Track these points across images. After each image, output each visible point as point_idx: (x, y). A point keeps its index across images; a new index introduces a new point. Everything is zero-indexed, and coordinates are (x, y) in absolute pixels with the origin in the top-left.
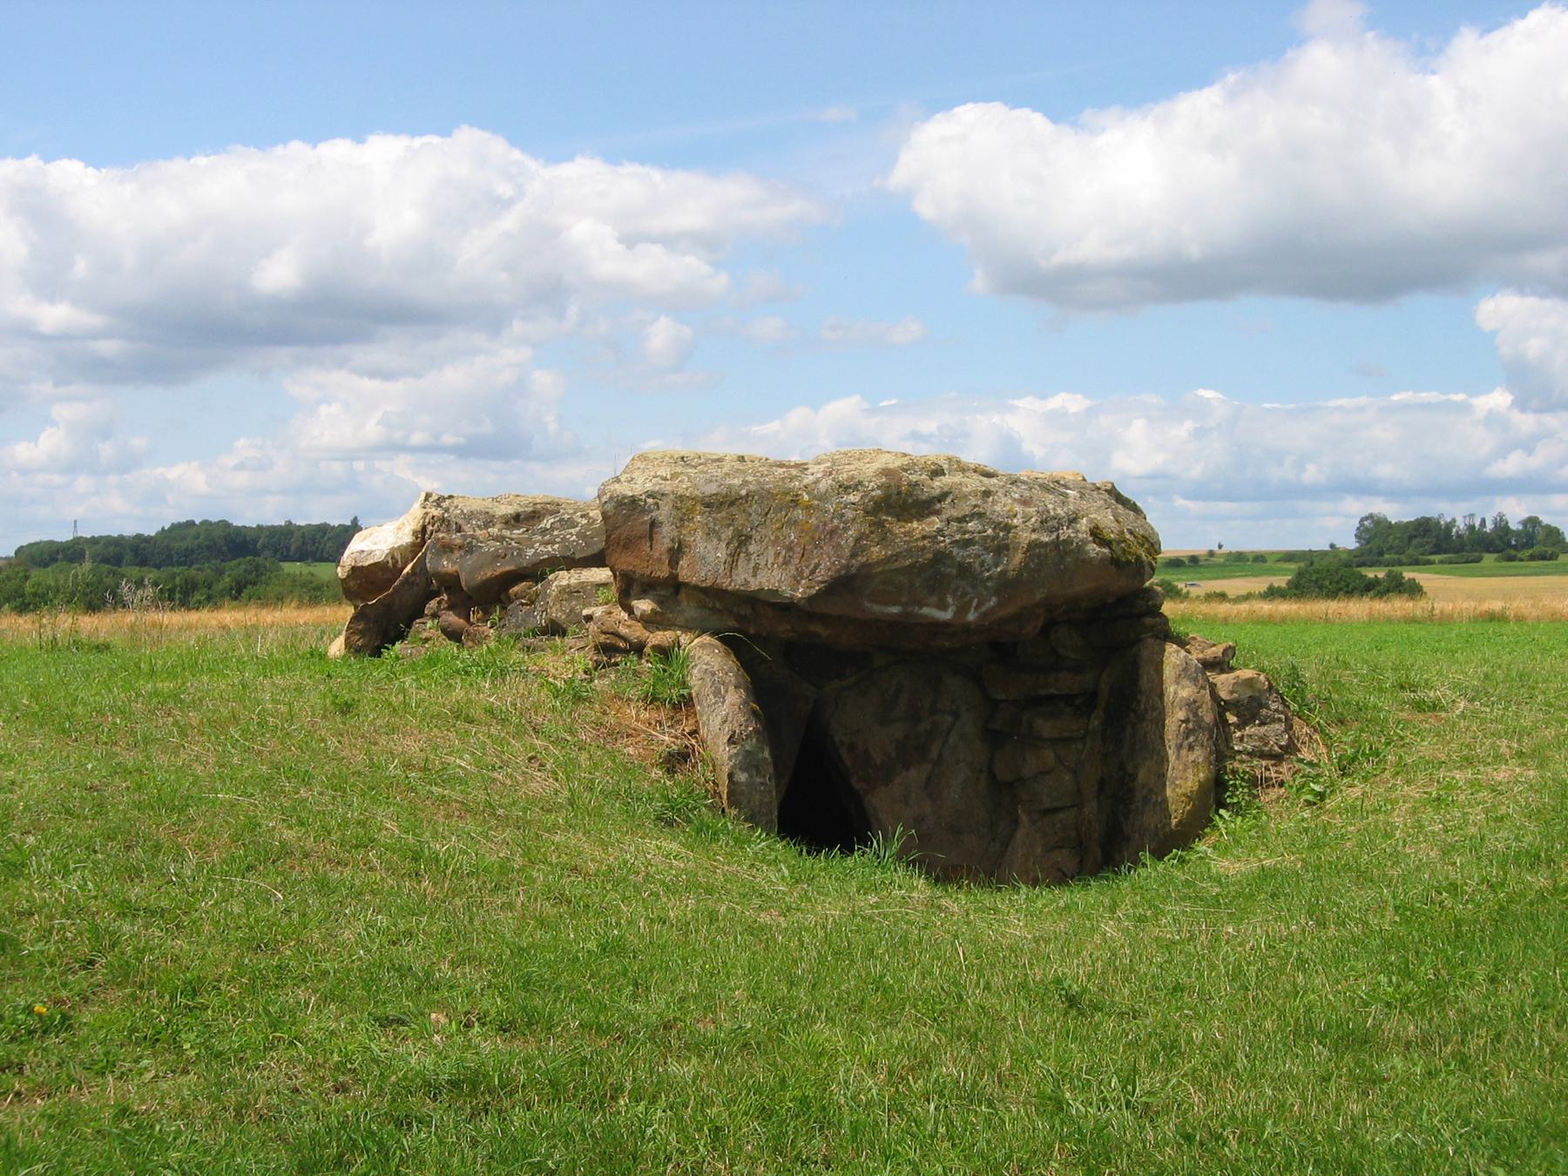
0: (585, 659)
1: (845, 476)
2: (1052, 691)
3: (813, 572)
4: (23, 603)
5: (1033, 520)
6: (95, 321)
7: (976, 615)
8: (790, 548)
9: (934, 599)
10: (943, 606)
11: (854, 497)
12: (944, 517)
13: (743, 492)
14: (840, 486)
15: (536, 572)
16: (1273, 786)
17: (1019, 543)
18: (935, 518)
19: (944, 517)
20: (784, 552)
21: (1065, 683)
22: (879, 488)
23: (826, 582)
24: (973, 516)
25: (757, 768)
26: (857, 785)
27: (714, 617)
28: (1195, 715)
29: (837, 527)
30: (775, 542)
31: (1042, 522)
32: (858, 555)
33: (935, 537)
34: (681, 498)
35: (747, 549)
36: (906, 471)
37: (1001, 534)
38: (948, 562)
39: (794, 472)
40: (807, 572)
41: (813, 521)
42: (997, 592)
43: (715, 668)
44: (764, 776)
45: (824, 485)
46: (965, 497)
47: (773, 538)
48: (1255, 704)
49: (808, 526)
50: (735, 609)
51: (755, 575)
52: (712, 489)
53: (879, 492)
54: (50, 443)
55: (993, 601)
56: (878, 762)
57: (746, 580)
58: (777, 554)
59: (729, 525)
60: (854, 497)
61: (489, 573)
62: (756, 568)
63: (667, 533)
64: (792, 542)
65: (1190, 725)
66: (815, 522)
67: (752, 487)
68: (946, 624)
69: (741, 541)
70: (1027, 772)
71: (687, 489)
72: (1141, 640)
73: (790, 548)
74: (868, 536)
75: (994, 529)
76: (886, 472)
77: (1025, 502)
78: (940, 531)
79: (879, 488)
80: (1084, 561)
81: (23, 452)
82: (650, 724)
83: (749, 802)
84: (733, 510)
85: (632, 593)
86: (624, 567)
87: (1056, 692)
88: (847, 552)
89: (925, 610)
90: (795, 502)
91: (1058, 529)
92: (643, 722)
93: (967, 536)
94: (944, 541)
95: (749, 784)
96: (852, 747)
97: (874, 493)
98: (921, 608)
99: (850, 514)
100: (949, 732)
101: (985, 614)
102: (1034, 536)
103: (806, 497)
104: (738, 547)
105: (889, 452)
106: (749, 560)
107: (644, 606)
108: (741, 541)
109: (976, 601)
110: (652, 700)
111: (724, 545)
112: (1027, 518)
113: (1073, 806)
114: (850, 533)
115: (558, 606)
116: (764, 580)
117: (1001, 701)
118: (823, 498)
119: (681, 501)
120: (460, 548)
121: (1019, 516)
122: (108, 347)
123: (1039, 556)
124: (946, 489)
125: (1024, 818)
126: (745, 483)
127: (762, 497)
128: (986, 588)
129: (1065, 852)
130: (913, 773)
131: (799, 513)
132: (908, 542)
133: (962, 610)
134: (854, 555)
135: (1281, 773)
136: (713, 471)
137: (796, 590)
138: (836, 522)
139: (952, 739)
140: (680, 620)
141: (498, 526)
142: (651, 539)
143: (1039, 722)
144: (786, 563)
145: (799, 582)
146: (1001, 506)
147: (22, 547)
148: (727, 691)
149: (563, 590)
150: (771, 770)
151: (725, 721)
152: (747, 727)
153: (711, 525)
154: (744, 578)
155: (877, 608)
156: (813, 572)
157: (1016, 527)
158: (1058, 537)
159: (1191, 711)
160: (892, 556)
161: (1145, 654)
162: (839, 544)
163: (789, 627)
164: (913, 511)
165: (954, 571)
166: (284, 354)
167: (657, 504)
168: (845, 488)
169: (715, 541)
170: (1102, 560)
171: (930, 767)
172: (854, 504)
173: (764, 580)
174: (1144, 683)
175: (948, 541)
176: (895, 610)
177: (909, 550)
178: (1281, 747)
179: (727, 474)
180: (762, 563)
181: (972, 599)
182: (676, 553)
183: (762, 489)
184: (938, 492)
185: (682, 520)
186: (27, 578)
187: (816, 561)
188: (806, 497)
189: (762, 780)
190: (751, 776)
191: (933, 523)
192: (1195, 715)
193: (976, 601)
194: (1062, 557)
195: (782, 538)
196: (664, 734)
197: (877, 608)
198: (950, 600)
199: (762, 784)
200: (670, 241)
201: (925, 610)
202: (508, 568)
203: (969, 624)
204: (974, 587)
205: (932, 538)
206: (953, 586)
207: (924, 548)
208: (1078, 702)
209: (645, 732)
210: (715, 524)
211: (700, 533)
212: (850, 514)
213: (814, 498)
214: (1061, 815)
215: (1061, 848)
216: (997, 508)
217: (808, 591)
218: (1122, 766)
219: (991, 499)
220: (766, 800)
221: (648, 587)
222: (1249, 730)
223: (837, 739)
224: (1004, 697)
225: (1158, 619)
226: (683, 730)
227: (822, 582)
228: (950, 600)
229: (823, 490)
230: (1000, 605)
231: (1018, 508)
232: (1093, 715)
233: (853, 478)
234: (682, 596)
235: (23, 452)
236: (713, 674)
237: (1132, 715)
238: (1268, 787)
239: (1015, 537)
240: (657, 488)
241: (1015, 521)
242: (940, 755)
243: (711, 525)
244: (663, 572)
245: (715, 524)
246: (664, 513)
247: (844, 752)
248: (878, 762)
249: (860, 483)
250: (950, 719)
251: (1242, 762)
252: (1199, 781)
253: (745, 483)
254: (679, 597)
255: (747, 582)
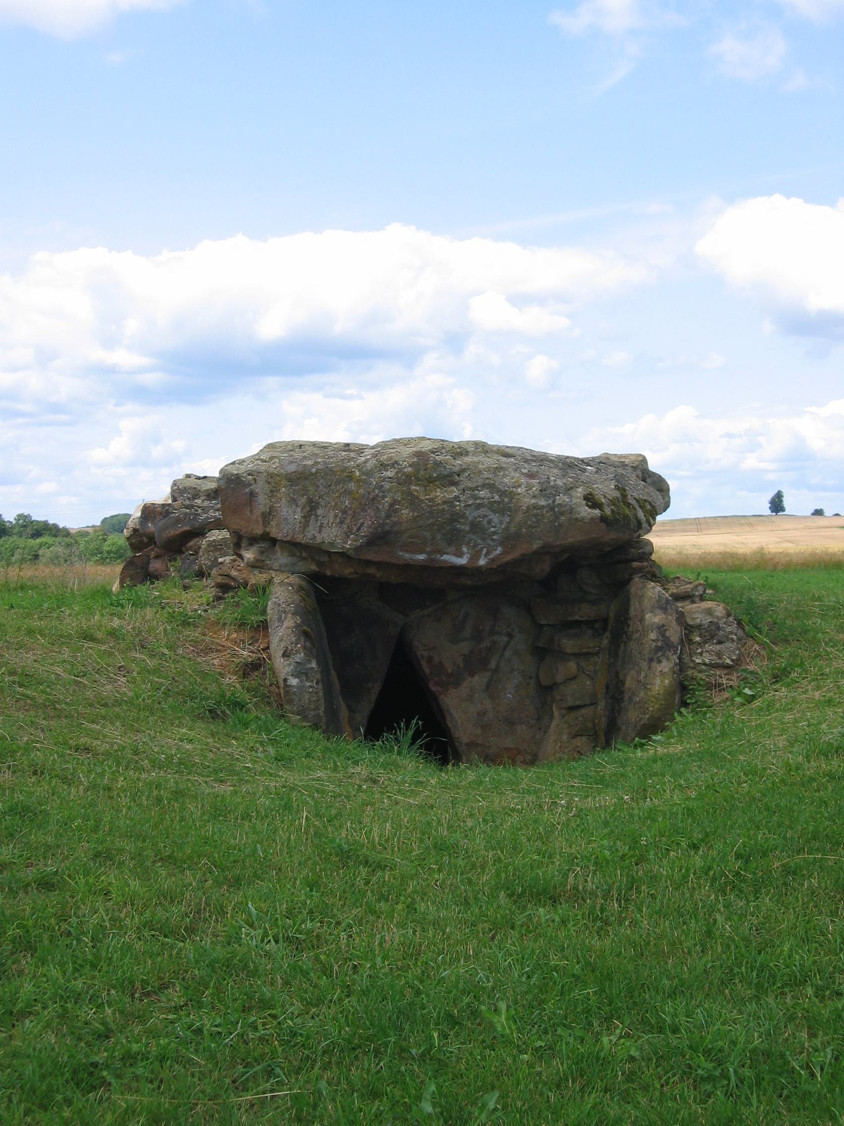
0: (210, 593)
1: (385, 457)
2: (577, 617)
3: (359, 529)
4: (102, 558)
5: (534, 489)
6: (145, 361)
7: (486, 560)
8: (344, 512)
9: (452, 549)
10: (460, 555)
11: (390, 473)
12: (461, 487)
13: (314, 470)
14: (381, 465)
15: (199, 532)
16: (724, 689)
17: (521, 506)
18: (454, 488)
19: (461, 487)
20: (340, 514)
21: (586, 612)
22: (410, 466)
23: (367, 536)
24: (484, 486)
25: (306, 674)
26: (434, 689)
27: (301, 563)
28: (663, 635)
29: (377, 495)
30: (334, 508)
31: (541, 491)
32: (391, 516)
33: (452, 502)
34: (271, 475)
35: (316, 512)
36: (434, 453)
37: (506, 500)
38: (463, 521)
39: (352, 455)
40: (355, 529)
41: (361, 491)
42: (502, 543)
43: (282, 601)
44: (312, 681)
45: (369, 465)
46: (480, 472)
47: (333, 504)
48: (713, 627)
49: (358, 494)
50: (317, 557)
51: (320, 532)
52: (292, 468)
53: (410, 469)
54: (120, 446)
55: (499, 550)
56: (450, 671)
57: (313, 535)
58: (336, 516)
59: (303, 495)
60: (390, 473)
61: (172, 532)
62: (321, 527)
63: (262, 502)
64: (347, 507)
65: (659, 644)
66: (363, 492)
67: (320, 466)
68: (462, 567)
69: (312, 507)
70: (559, 678)
71: (276, 468)
72: (632, 578)
73: (344, 512)
74: (399, 502)
75: (500, 496)
76: (419, 454)
77: (531, 475)
78: (456, 498)
79: (410, 466)
80: (576, 519)
81: (98, 454)
82: (235, 642)
83: (300, 700)
84: (307, 483)
85: (243, 545)
86: (235, 526)
87: (580, 619)
88: (383, 514)
89: (445, 557)
90: (350, 478)
91: (555, 495)
92: (231, 641)
93: (478, 502)
94: (460, 505)
95: (301, 687)
96: (430, 660)
97: (406, 470)
98: (442, 556)
99: (387, 486)
100: (505, 649)
101: (493, 560)
102: (533, 501)
103: (358, 474)
104: (309, 511)
105: (429, 439)
106: (317, 520)
107: (249, 555)
108: (312, 507)
109: (485, 550)
110: (241, 625)
111: (299, 509)
112: (529, 487)
113: (591, 704)
114: (386, 500)
115: (206, 556)
116: (325, 535)
117: (543, 626)
118: (369, 474)
119: (272, 477)
120: (161, 514)
121: (523, 486)
122: (151, 379)
123: (535, 516)
124: (464, 467)
125: (556, 713)
126: (316, 463)
127: (326, 474)
128: (493, 540)
129: (584, 739)
130: (476, 678)
131: (352, 486)
132: (432, 506)
133: (475, 556)
134: (388, 516)
135: (731, 680)
136: (298, 455)
137: (346, 543)
138: (377, 491)
139: (507, 654)
140: (276, 565)
141: (203, 498)
142: (251, 504)
143: (564, 641)
144: (341, 522)
145: (348, 537)
146: (507, 480)
147: (106, 518)
148: (285, 618)
149: (210, 544)
150: (319, 676)
151: (282, 640)
152: (296, 644)
153: (292, 495)
154: (312, 535)
155: (407, 556)
156: (359, 529)
157: (519, 494)
158: (554, 501)
159: (660, 633)
160: (417, 516)
161: (633, 590)
162: (378, 508)
163: (352, 570)
164: (438, 483)
165: (467, 528)
166: (272, 381)
167: (255, 479)
168: (383, 466)
169: (294, 506)
170: (592, 519)
171: (489, 674)
172: (390, 478)
173: (325, 535)
174: (632, 612)
175: (463, 505)
176: (422, 557)
177: (431, 512)
178: (732, 660)
179: (305, 457)
180: (325, 522)
181: (482, 549)
182: (266, 517)
183: (327, 467)
184: (456, 469)
185: (273, 492)
186: (105, 540)
187: (362, 521)
188: (358, 474)
189: (310, 684)
190: (301, 681)
191: (453, 491)
192: (663, 635)
193: (485, 550)
194: (557, 517)
195: (339, 504)
196: (243, 649)
197: (407, 556)
198: (465, 549)
199: (311, 687)
200: (539, 300)
201: (445, 557)
202: (186, 528)
203: (481, 567)
204: (483, 540)
205: (450, 502)
206: (467, 539)
207: (443, 510)
208: (597, 626)
209: (230, 648)
210: (294, 494)
211: (284, 501)
212: (387, 486)
213: (363, 474)
214: (583, 711)
215: (581, 735)
216: (506, 480)
217: (354, 543)
218: (617, 673)
219: (502, 473)
220: (315, 699)
221: (253, 540)
222: (707, 647)
223: (419, 654)
224: (546, 623)
225: (645, 564)
226: (259, 646)
227: (365, 537)
228: (465, 549)
229: (369, 468)
230: (504, 553)
231: (523, 480)
232: (605, 636)
233: (391, 458)
234: (277, 548)
235: (98, 454)
236: (279, 605)
237: (624, 636)
238: (720, 691)
239: (518, 502)
240: (255, 468)
241: (519, 490)
242: (498, 667)
243: (292, 495)
244: (259, 531)
245: (294, 494)
246: (260, 488)
247: (424, 663)
248: (450, 671)
249: (396, 462)
250: (506, 639)
251: (700, 672)
252: (664, 686)
253: (316, 463)
254: (276, 548)
255: (314, 537)
